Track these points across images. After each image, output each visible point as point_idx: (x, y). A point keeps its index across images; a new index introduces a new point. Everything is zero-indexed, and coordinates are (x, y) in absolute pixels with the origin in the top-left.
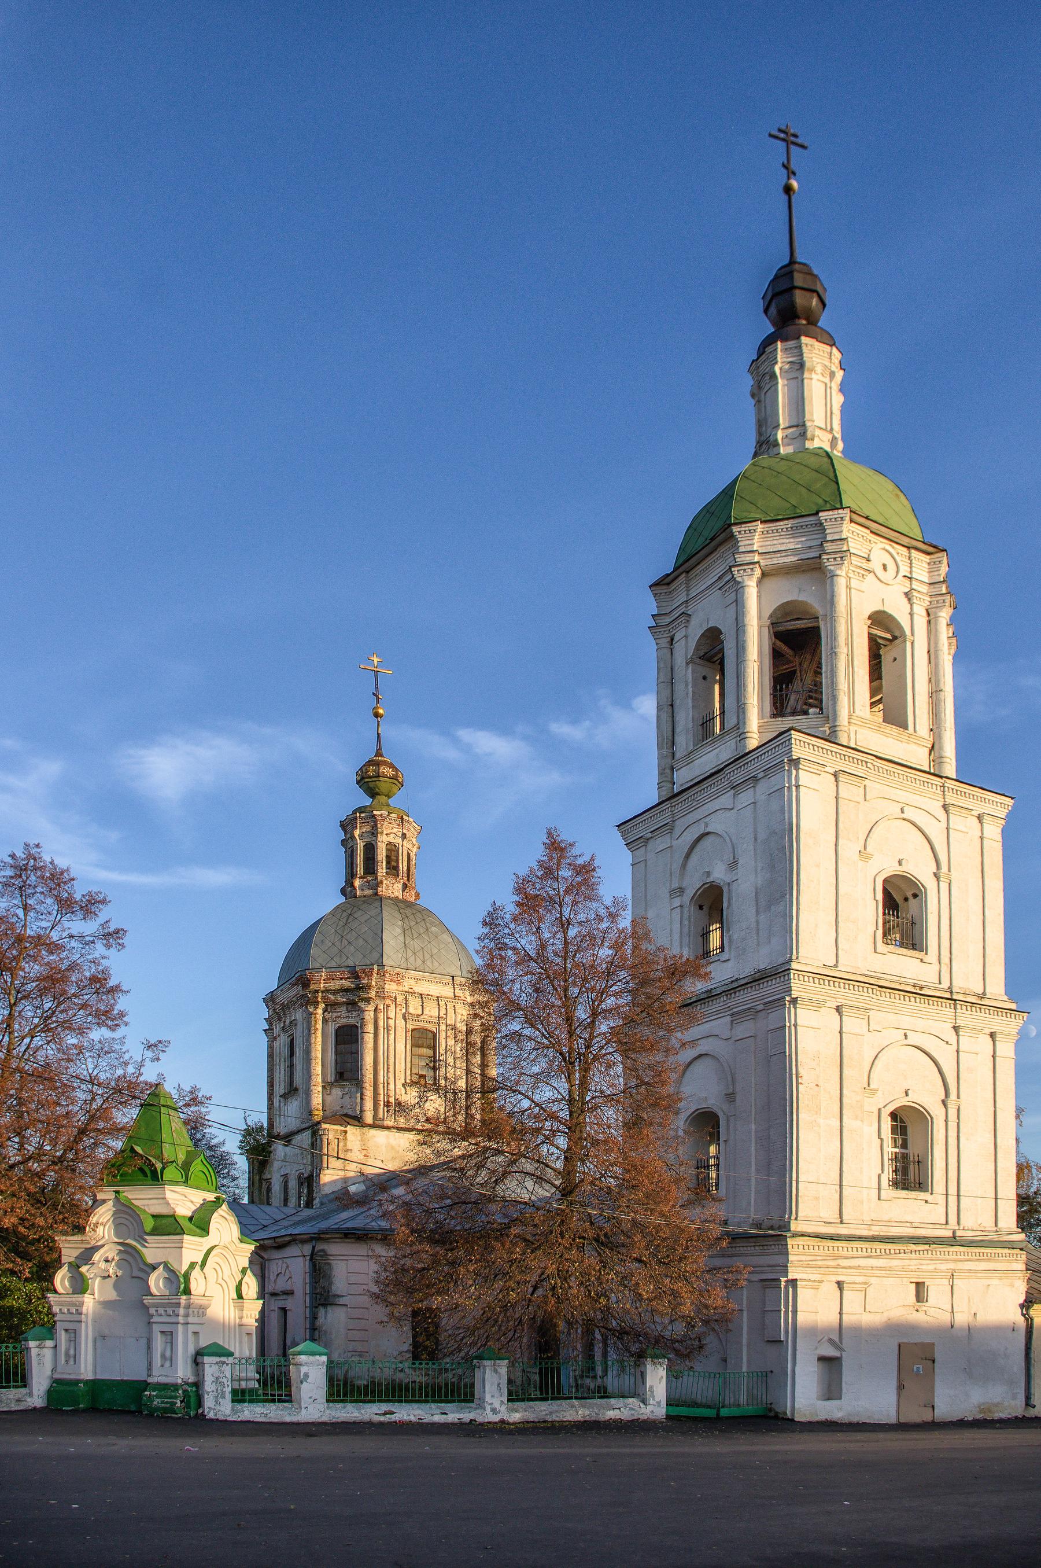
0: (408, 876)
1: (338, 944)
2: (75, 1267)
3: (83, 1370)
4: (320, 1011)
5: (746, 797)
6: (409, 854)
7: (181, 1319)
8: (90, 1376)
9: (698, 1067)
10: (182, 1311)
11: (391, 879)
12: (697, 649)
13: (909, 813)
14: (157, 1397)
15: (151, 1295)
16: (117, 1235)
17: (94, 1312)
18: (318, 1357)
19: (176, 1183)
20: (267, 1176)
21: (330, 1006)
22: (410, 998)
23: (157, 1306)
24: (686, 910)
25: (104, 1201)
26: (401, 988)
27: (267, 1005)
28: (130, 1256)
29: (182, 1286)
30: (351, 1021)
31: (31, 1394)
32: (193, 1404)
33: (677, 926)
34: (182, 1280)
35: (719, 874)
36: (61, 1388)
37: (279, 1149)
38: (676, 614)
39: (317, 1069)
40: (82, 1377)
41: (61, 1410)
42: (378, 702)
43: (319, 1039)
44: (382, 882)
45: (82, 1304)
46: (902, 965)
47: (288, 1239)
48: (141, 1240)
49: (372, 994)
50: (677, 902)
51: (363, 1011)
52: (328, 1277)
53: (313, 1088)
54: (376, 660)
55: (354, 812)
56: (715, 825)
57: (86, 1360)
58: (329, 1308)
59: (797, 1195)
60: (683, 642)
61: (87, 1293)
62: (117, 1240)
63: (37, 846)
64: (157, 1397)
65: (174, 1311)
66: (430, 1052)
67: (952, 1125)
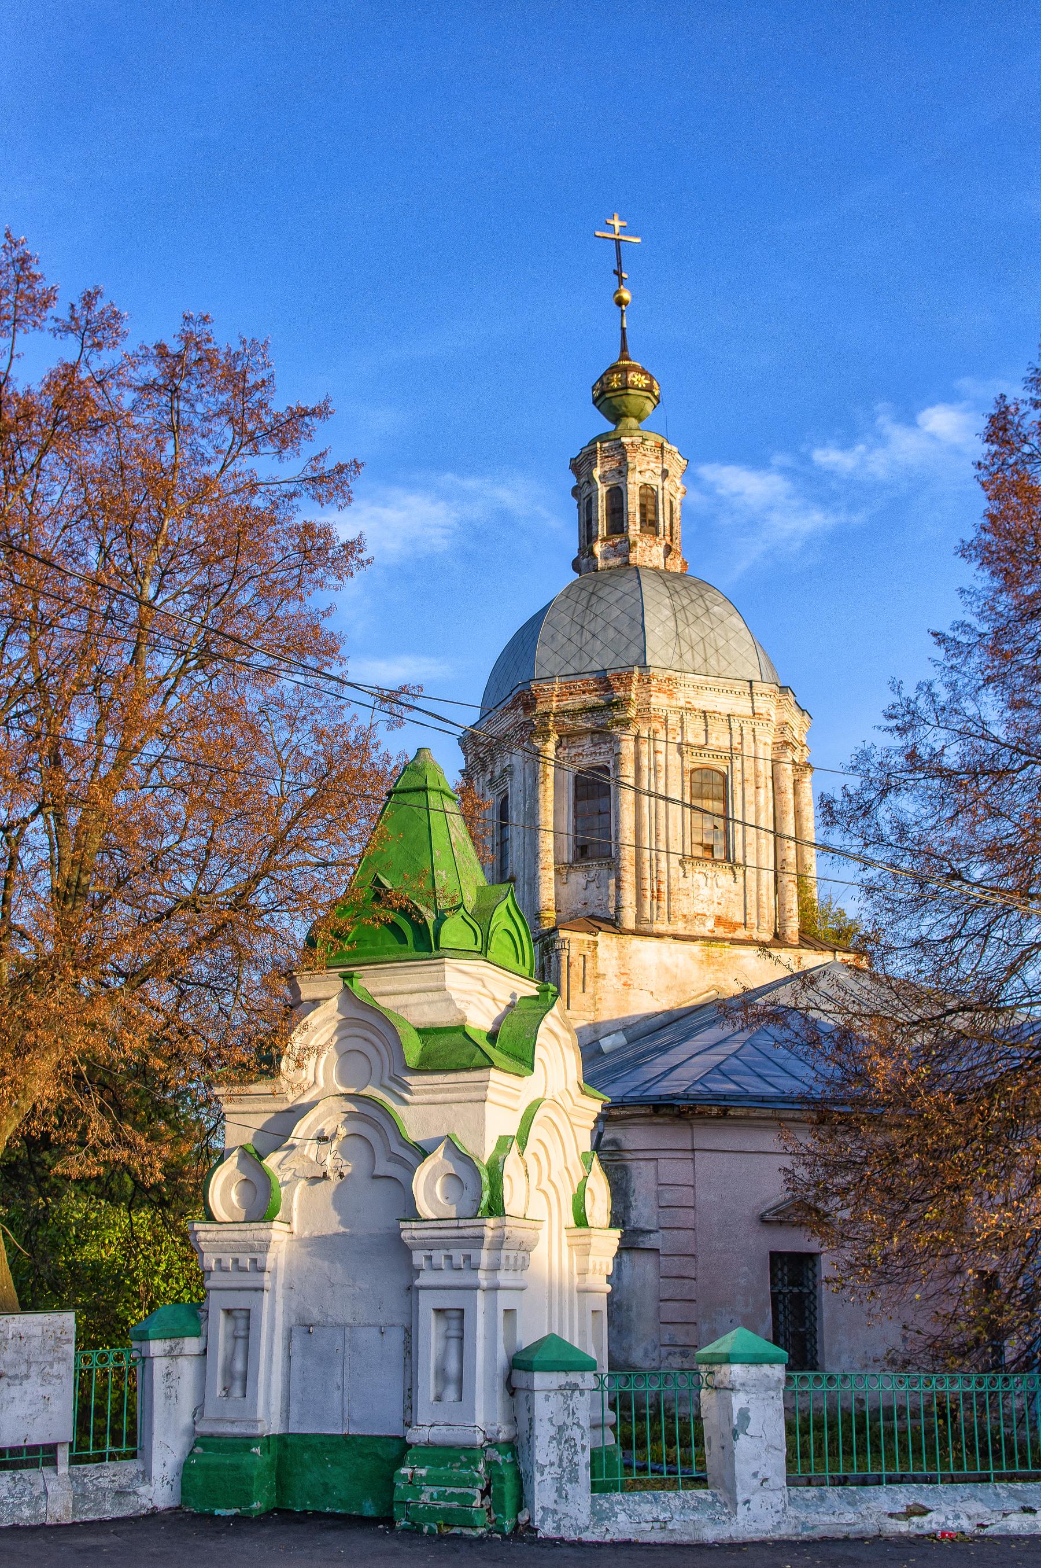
0: (671, 535)
1: (576, 638)
2: (253, 1158)
3: (260, 1414)
4: (551, 746)
6: (671, 503)
7: (483, 1278)
8: (275, 1428)
10: (485, 1257)
11: (647, 539)
14: (430, 1481)
15: (416, 1217)
16: (343, 1081)
17: (289, 1263)
18: (766, 1368)
19: (465, 953)
21: (566, 739)
22: (687, 718)
23: (429, 1245)
25: (316, 1003)
26: (674, 703)
27: (464, 750)
28: (371, 1122)
29: (486, 1195)
30: (600, 760)
31: (146, 1475)
32: (509, 1504)
34: (485, 1179)
36: (214, 1458)
39: (547, 842)
40: (260, 1430)
41: (211, 1516)
43: (551, 792)
44: (635, 544)
45: (265, 1246)
48: (397, 1085)
49: (632, 713)
51: (618, 742)
53: (541, 873)
54: (617, 223)
55: (593, 442)
57: (269, 1385)
61: (276, 1213)
62: (342, 1090)
63: (205, 319)
64: (430, 1481)
65: (468, 1258)
66: (717, 807)
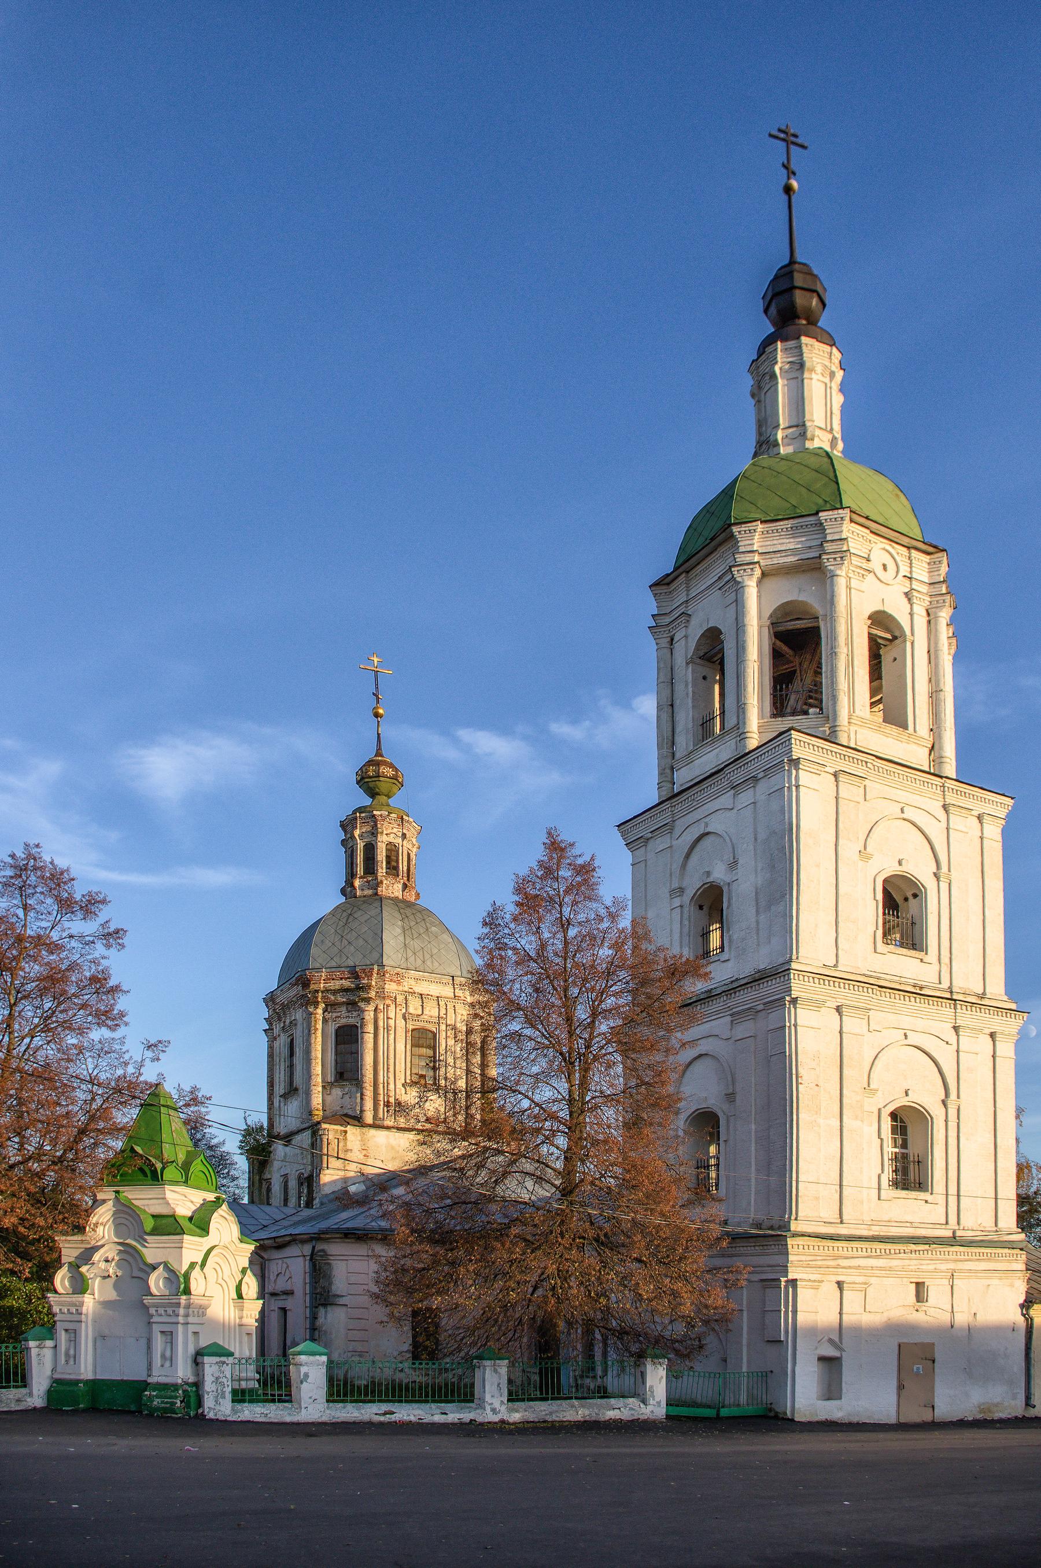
0: (408, 876)
1: (338, 944)
2: (75, 1267)
3: (83, 1370)
4: (320, 1011)
5: (746, 797)
6: (409, 854)
7: (181, 1319)
8: (90, 1376)
9: (698, 1067)
10: (182, 1311)
11: (391, 879)
12: (697, 649)
13: (909, 813)
14: (157, 1397)
15: (151, 1295)
16: (117, 1235)
17: (94, 1312)
18: (318, 1357)
19: (176, 1183)
20: (267, 1176)
21: (330, 1006)
22: (410, 998)
23: (157, 1306)
24: (686, 910)
25: (104, 1201)
26: (401, 988)
27: (267, 1005)
28: (130, 1256)
29: (182, 1286)
30: (351, 1021)
31: (31, 1394)
32: (193, 1404)
33: (677, 926)
34: (182, 1280)
35: (719, 874)
36: (61, 1388)
37: (279, 1149)
38: (676, 614)
39: (317, 1069)
40: (82, 1377)
41: (61, 1410)
42: (378, 702)
43: (319, 1039)
44: (382, 882)
45: (82, 1304)
46: (902, 965)
47: (288, 1239)
48: (141, 1240)
49: (372, 994)
50: (677, 902)
51: (363, 1011)
52: (328, 1277)
53: (313, 1088)
54: (376, 660)
55: (354, 812)
56: (715, 825)
57: (86, 1360)
58: (329, 1308)
59: (797, 1195)
60: (683, 642)
61: (87, 1293)
62: (117, 1240)
63: (37, 846)
64: (157, 1397)
65: (174, 1311)
66: (430, 1052)
67: (952, 1125)
